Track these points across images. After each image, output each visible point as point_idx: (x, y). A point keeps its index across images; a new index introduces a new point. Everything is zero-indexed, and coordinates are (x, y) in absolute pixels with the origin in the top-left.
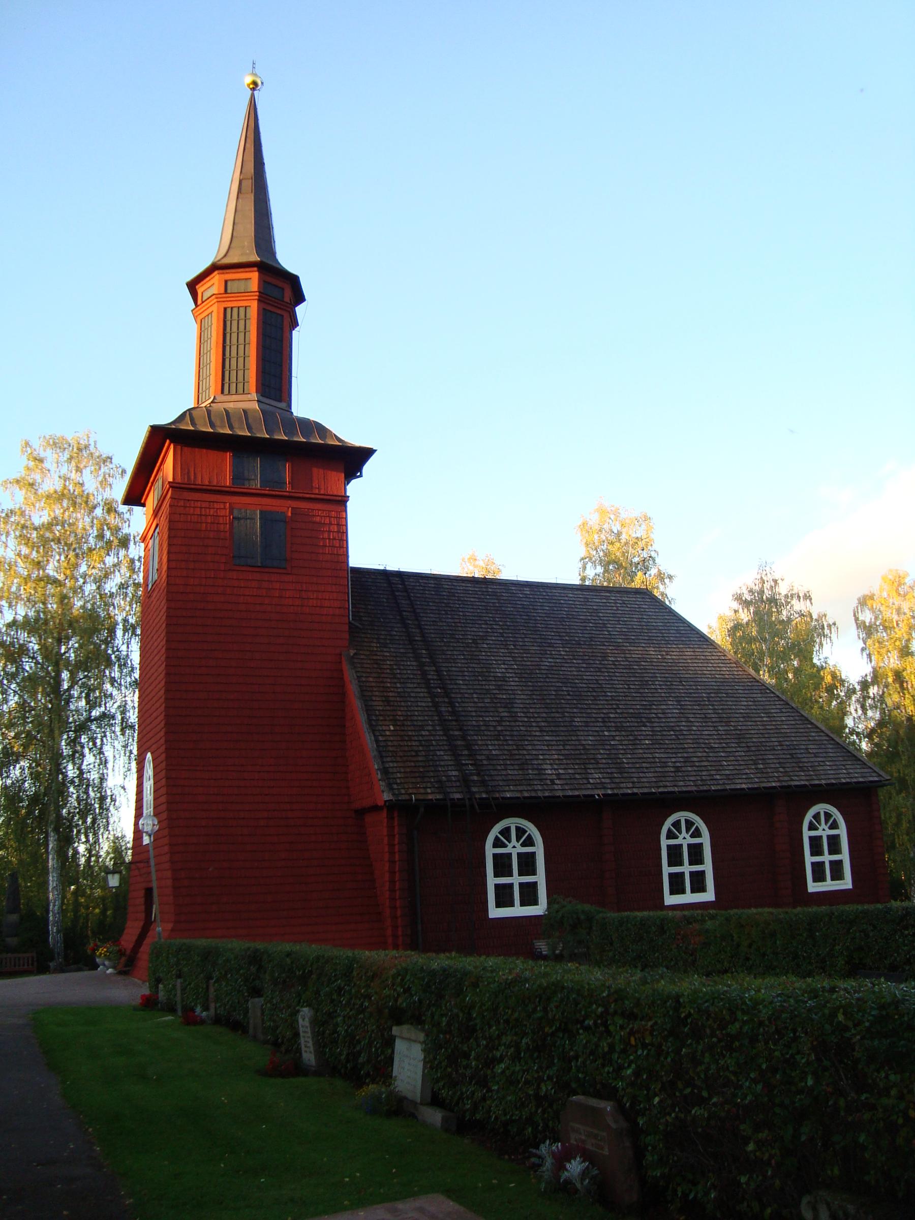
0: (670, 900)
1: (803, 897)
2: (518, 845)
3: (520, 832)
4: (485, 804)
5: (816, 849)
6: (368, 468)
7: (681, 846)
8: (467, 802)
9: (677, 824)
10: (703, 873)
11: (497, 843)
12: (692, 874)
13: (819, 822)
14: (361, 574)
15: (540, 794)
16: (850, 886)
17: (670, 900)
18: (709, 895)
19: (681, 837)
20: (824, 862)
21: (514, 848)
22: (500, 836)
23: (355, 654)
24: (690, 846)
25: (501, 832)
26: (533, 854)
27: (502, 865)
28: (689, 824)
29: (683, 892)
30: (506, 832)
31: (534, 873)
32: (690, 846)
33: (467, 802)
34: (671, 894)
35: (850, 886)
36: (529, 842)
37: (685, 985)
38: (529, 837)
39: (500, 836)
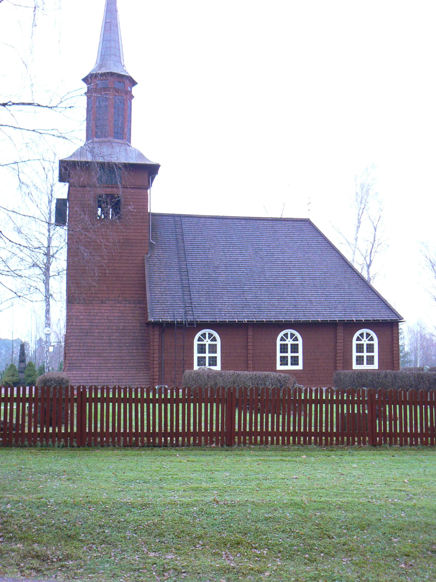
0: (279, 367)
1: (276, 371)
2: (367, 340)
3: (210, 335)
4: (191, 324)
5: (360, 348)
6: (160, 171)
7: (363, 344)
8: (184, 322)
9: (362, 335)
10: (298, 357)
11: (358, 339)
12: (292, 357)
13: (363, 337)
15: (218, 320)
16: (377, 368)
17: (279, 367)
18: (300, 367)
19: (363, 340)
21: (365, 342)
22: (201, 337)
24: (292, 345)
25: (202, 335)
26: (216, 345)
27: (284, 348)
28: (368, 335)
29: (287, 364)
30: (204, 335)
31: (216, 352)
32: (292, 345)
33: (184, 322)
34: (281, 365)
35: (377, 368)
36: (372, 339)
38: (372, 337)
39: (201, 337)
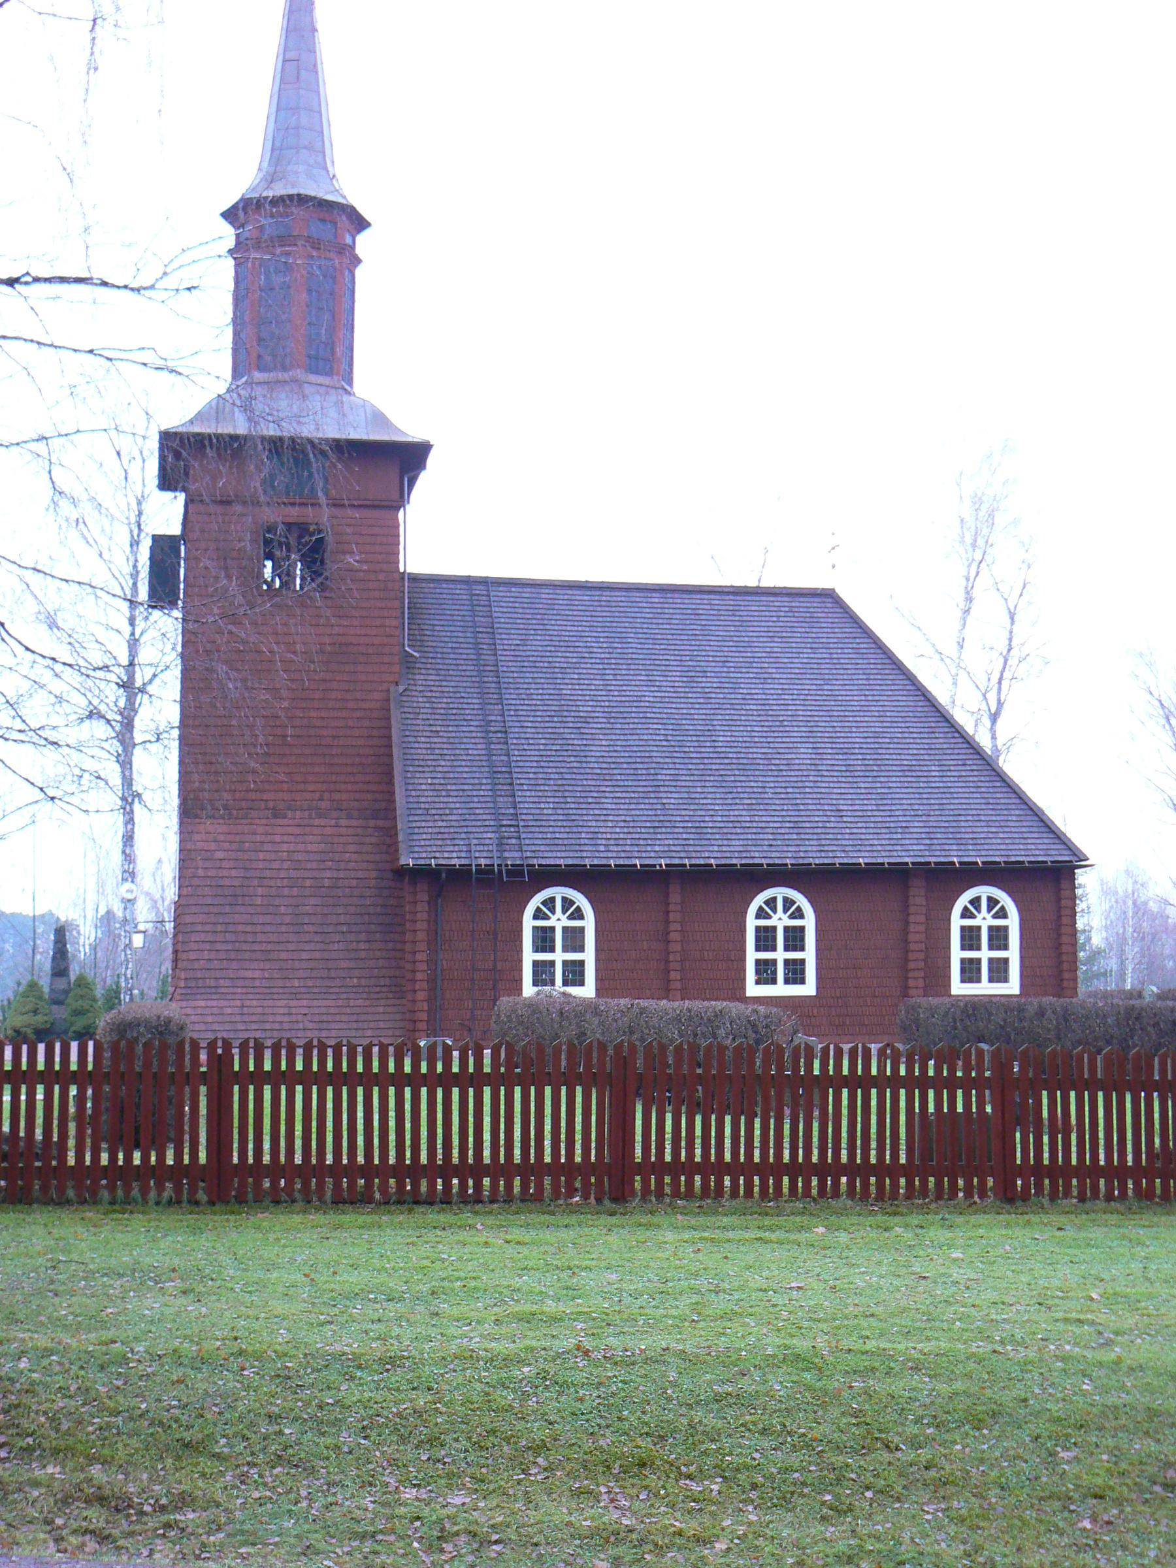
0: (753, 990)
2: (989, 916)
3: (567, 903)
4: (516, 872)
7: (979, 928)
8: (496, 867)
9: (976, 902)
10: (803, 962)
11: (966, 914)
12: (787, 962)
13: (978, 909)
14: (415, 579)
15: (587, 862)
16: (1016, 991)
17: (753, 990)
18: (809, 988)
19: (980, 917)
20: (564, 951)
21: (984, 920)
22: (542, 907)
23: (405, 690)
24: (787, 929)
25: (544, 903)
26: (582, 930)
27: (765, 939)
28: (992, 902)
29: (774, 981)
30: (550, 903)
31: (581, 949)
32: (787, 929)
34: (758, 982)
35: (1016, 991)
36: (1002, 914)
37: (107, 1018)
38: (1003, 908)
39: (542, 907)
